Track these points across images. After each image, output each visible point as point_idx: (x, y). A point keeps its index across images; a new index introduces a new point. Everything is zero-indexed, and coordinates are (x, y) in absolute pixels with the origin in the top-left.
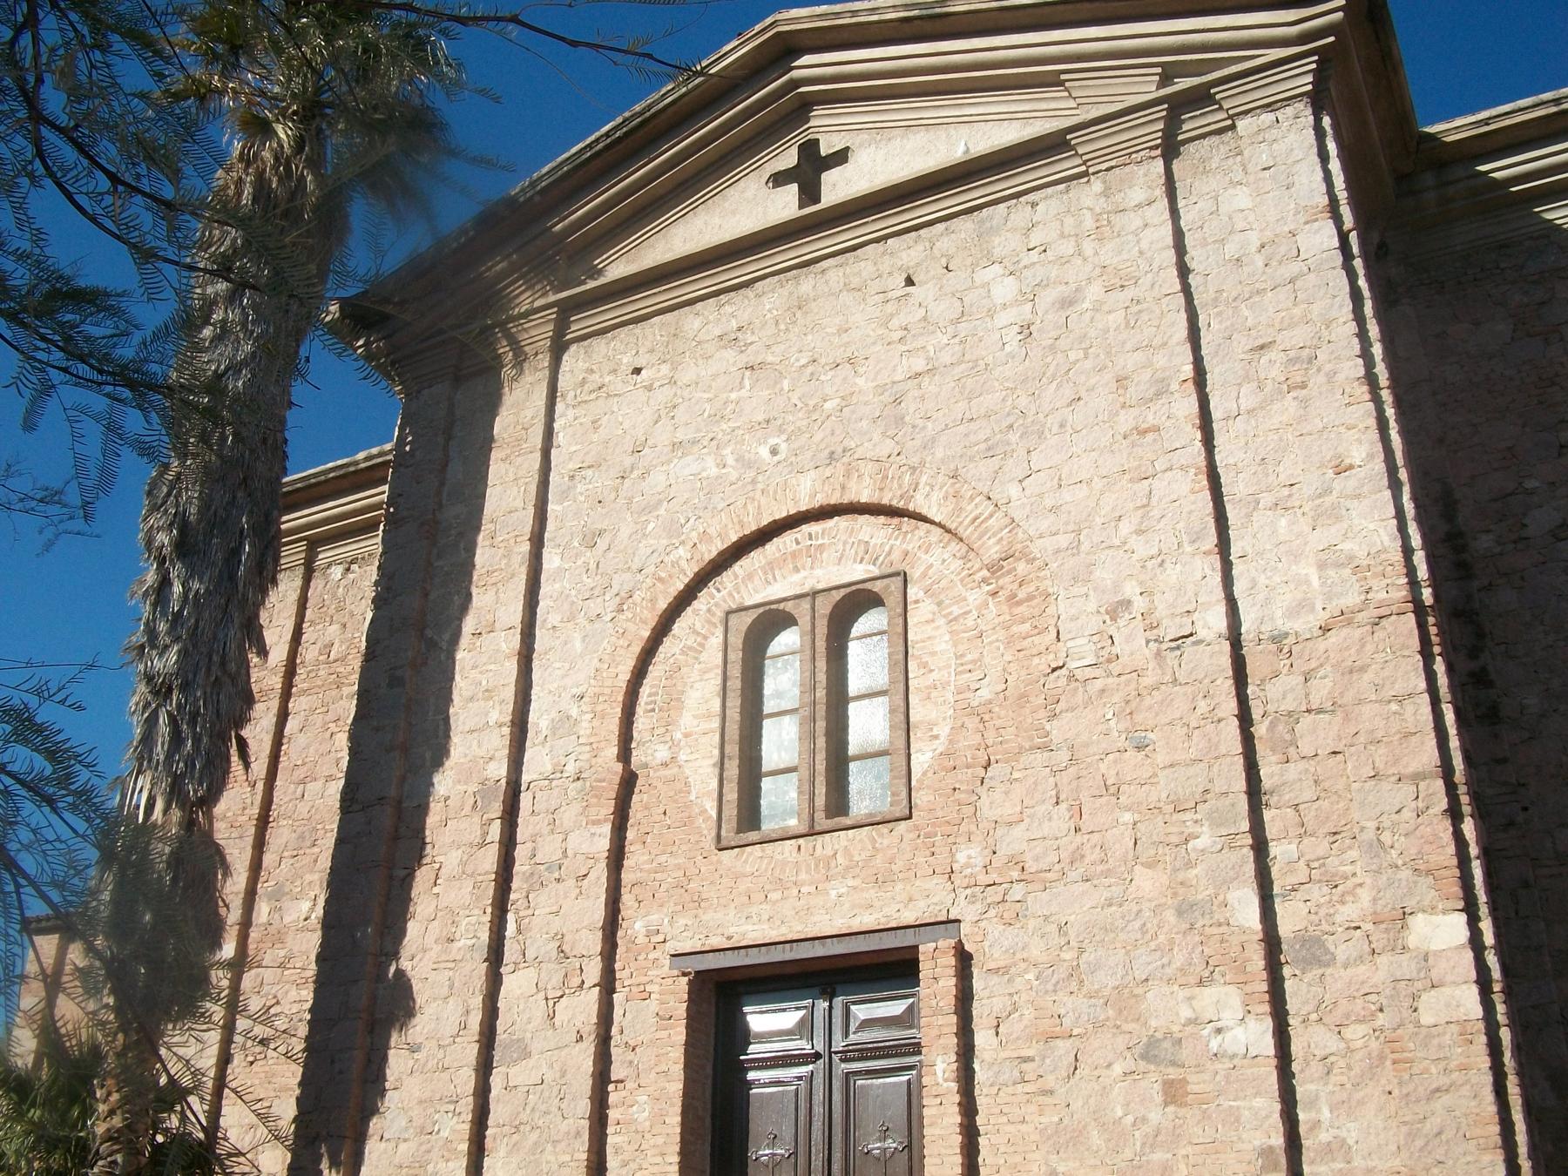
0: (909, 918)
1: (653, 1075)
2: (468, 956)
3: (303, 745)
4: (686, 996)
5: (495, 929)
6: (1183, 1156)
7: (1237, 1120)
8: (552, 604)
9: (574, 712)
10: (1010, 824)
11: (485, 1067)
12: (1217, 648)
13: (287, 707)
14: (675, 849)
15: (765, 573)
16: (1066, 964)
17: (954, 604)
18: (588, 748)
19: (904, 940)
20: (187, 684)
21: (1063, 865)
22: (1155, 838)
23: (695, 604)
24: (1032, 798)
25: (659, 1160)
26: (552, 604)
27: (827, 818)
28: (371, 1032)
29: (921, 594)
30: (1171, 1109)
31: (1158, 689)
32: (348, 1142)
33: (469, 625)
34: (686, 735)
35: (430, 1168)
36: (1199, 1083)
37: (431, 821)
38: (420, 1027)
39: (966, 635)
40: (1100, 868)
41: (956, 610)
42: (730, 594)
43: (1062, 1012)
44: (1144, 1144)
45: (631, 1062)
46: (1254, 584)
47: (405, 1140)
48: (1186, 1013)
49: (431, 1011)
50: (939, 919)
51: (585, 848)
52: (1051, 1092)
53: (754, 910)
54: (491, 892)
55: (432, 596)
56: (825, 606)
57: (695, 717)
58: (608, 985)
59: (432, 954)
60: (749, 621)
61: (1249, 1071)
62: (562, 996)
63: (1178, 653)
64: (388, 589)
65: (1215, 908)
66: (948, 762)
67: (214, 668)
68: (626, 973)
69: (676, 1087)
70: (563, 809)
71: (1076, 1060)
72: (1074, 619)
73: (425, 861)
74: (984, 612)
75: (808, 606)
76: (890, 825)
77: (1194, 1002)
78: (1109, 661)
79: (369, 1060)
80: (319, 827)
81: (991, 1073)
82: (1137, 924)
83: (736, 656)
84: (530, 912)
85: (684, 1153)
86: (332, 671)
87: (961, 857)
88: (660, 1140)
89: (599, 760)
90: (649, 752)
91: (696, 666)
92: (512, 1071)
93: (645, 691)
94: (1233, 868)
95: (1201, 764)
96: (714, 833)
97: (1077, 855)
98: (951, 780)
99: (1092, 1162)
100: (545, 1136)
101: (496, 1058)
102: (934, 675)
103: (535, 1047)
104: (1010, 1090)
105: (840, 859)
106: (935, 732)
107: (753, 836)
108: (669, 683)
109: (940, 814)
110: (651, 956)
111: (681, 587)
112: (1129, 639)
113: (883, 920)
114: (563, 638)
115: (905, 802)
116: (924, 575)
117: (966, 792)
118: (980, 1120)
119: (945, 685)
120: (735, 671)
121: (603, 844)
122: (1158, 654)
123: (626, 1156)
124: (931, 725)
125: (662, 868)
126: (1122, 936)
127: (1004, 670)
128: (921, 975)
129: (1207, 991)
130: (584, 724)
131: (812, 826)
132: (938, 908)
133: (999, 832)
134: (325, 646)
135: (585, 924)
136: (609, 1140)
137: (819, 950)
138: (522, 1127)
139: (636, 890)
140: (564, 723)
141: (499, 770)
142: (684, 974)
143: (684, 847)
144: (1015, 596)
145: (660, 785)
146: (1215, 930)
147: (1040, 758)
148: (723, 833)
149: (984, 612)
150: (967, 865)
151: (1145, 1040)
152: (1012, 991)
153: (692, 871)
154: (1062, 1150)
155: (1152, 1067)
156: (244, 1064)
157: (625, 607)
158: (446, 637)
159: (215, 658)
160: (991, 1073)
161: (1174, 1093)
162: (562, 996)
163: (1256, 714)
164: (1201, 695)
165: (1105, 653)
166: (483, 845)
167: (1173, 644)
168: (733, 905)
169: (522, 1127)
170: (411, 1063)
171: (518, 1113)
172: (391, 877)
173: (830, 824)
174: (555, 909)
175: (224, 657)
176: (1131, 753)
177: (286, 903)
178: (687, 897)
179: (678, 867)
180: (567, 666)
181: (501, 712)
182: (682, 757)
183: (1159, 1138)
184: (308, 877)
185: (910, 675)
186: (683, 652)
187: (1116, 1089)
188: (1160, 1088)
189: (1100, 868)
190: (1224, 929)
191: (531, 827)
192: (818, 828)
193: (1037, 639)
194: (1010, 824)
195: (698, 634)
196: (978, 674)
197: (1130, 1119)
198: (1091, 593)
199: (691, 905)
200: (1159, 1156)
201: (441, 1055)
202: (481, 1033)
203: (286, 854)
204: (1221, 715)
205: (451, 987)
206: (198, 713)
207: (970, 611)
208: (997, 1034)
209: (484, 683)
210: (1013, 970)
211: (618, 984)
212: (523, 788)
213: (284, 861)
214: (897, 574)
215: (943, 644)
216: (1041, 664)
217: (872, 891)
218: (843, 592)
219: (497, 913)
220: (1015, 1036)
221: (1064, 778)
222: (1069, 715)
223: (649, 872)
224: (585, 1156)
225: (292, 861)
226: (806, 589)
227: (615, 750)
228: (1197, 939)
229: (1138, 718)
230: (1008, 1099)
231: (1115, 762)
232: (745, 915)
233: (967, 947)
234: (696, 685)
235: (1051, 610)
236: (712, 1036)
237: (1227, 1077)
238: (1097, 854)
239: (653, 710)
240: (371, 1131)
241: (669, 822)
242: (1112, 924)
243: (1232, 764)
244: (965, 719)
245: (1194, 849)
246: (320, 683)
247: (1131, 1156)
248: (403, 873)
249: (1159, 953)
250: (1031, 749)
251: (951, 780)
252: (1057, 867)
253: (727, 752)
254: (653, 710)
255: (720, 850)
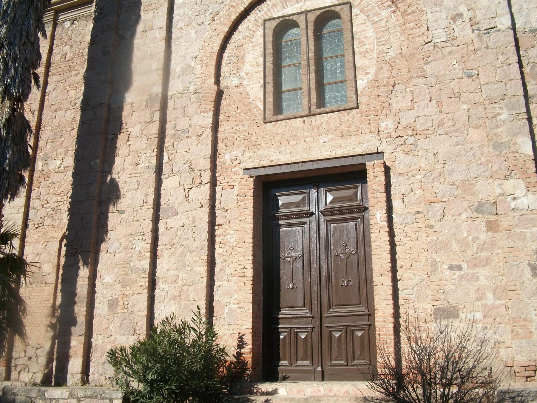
0: (359, 151)
1: (237, 221)
2: (146, 170)
3: (55, 96)
4: (253, 187)
5: (158, 159)
6: (496, 254)
7: (525, 238)
8: (180, 18)
9: (193, 64)
10: (406, 111)
11: (156, 219)
12: (507, 33)
13: (47, 81)
14: (243, 123)
15: (282, 4)
16: (437, 171)
17: (375, 16)
18: (200, 79)
19: (359, 161)
20: (11, 44)
21: (434, 128)
22: (478, 116)
23: (249, 17)
24: (418, 98)
25: (243, 258)
26: (180, 18)
27: (317, 108)
28: (100, 206)
29: (359, 12)
30: (490, 233)
31: (480, 50)
32: (91, 255)
33: (140, 28)
34: (247, 74)
35: (132, 264)
36: (506, 222)
37: (125, 113)
38: (123, 203)
39: (381, 29)
40: (452, 129)
41: (376, 19)
42: (266, 13)
43: (437, 191)
44: (478, 249)
45: (225, 216)
46: (521, 8)
47: (118, 253)
48: (499, 191)
49: (129, 195)
50: (373, 152)
51: (200, 123)
52: (433, 226)
53: (283, 149)
54: (156, 142)
55: (122, 16)
56: (312, 17)
57: (250, 66)
58: (213, 183)
59: (129, 171)
60: (275, 24)
61: (530, 216)
62: (192, 188)
63: (489, 35)
64: (100, 14)
65: (511, 145)
66: (375, 83)
67: (23, 38)
68: (222, 177)
69: (249, 226)
70: (188, 106)
71: (444, 212)
72: (436, 21)
73: (122, 131)
74: (390, 19)
75: (305, 17)
76: (348, 111)
77: (503, 186)
78: (453, 39)
79: (100, 218)
80: (63, 129)
81: (401, 219)
82: (471, 153)
83: (270, 39)
84: (175, 151)
85: (254, 255)
86: (67, 65)
87: (383, 125)
88: (243, 250)
89: (206, 85)
90: (229, 81)
91: (250, 44)
92: (169, 221)
93: (226, 55)
94: (519, 128)
95: (502, 83)
96: (262, 116)
97: (441, 123)
98: (376, 92)
99: (453, 257)
100: (186, 249)
101: (161, 216)
102: (367, 47)
103: (180, 210)
104: (411, 226)
105: (324, 126)
106: (368, 71)
107: (280, 117)
108: (237, 51)
109: (372, 106)
110: (234, 170)
111: (243, 9)
112: (462, 30)
113: (346, 153)
114: (185, 32)
115: (355, 101)
116: (360, 4)
117: (384, 96)
118: (396, 239)
119: (373, 50)
120: (270, 46)
121: (209, 120)
122: (479, 35)
123: (225, 257)
124: (366, 68)
125: (237, 131)
126: (464, 159)
127: (400, 44)
128: (368, 176)
129: (508, 182)
130: (197, 69)
131: (310, 112)
132: (373, 147)
133: (401, 114)
134: (63, 55)
135: (202, 156)
136: (216, 250)
137: (315, 166)
138: (175, 246)
139: (225, 141)
140: (188, 69)
141: (158, 89)
142: (251, 177)
143: (247, 122)
144: (406, 11)
145: (235, 96)
146: (511, 155)
147: (422, 81)
148: (267, 116)
149: (390, 19)
150: (386, 128)
151: (477, 203)
152: (410, 183)
153: (252, 132)
154: (438, 252)
155: (481, 215)
156: (34, 228)
157: (215, 19)
158: (129, 33)
159: (24, 33)
160: (401, 219)
161: (491, 227)
162: (192, 188)
163: (524, 63)
164: (500, 53)
165: (451, 36)
166: (151, 122)
167: (486, 31)
168: (273, 147)
169: (175, 246)
170: (120, 219)
171: (173, 239)
172: (107, 139)
173: (318, 111)
174: (187, 150)
175: (27, 33)
176: (465, 79)
177: (50, 161)
178: (250, 144)
179: (245, 131)
180: (188, 44)
181: (157, 64)
182: (245, 83)
183: (485, 246)
184: (59, 150)
185: (355, 47)
186: (243, 38)
187: (463, 225)
188: (485, 224)
189: (452, 129)
190: (515, 154)
191: (173, 115)
192: (312, 113)
193: (418, 30)
194: (406, 111)
195: (251, 30)
196: (388, 46)
197: (471, 238)
198: (443, 10)
199: (252, 147)
200: (484, 254)
201: (135, 214)
202: (154, 205)
203: (49, 141)
204: (510, 62)
205: (139, 184)
206: (16, 57)
207: (383, 19)
208: (403, 202)
209: (149, 52)
210: (410, 174)
211: (218, 183)
212: (169, 97)
213: (48, 144)
214: (347, 3)
215: (370, 33)
216: (420, 41)
217: (340, 140)
218: (320, 11)
219: (159, 152)
220: (412, 202)
221: (434, 90)
222: (435, 62)
223: (231, 133)
224: (206, 257)
225: (52, 144)
226: (303, 10)
227: (213, 80)
228: (503, 159)
229: (468, 64)
230: (410, 230)
231: (458, 83)
232: (279, 151)
233: (387, 164)
234: (251, 52)
235: (424, 17)
236: (262, 205)
237: (519, 219)
238: (451, 123)
239: (230, 63)
240: (102, 249)
241: (240, 111)
242: (459, 153)
243: (516, 83)
244: (383, 65)
245: (500, 120)
246: (62, 70)
247: (472, 254)
248: (112, 136)
249: (482, 166)
250: (417, 77)
251: (376, 92)
252: (432, 128)
253: (266, 80)
254: (230, 63)
255: (265, 123)
